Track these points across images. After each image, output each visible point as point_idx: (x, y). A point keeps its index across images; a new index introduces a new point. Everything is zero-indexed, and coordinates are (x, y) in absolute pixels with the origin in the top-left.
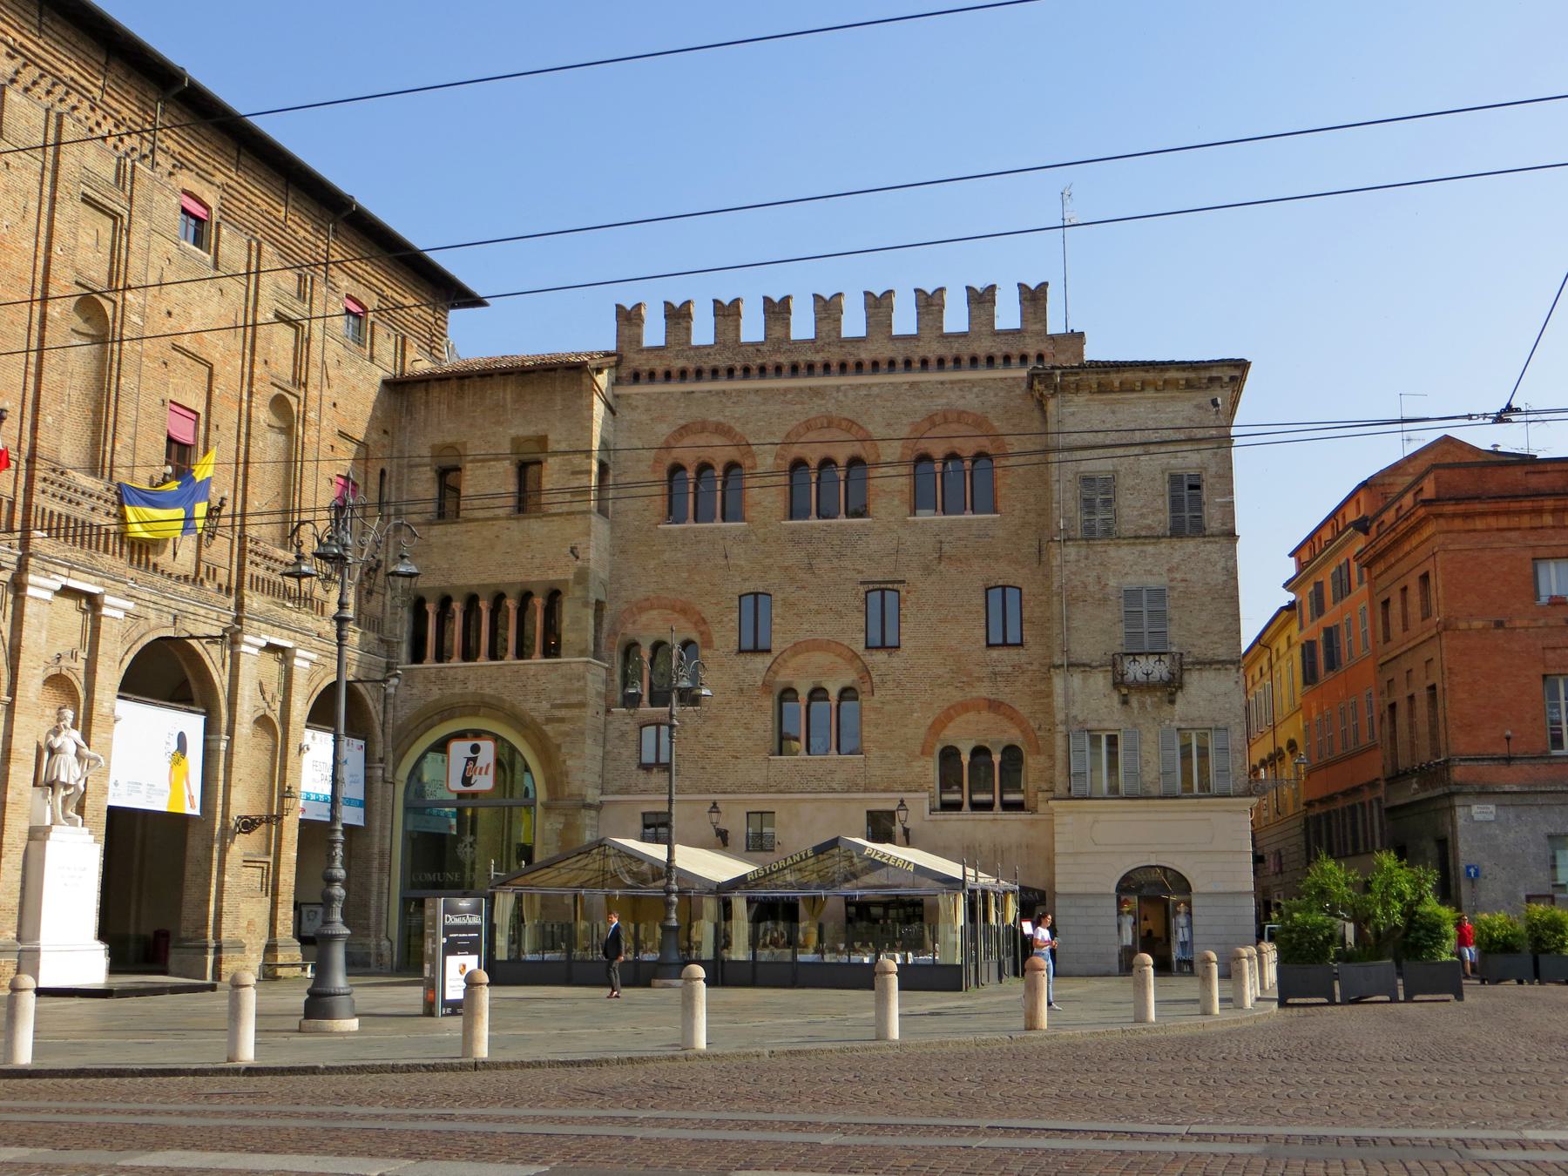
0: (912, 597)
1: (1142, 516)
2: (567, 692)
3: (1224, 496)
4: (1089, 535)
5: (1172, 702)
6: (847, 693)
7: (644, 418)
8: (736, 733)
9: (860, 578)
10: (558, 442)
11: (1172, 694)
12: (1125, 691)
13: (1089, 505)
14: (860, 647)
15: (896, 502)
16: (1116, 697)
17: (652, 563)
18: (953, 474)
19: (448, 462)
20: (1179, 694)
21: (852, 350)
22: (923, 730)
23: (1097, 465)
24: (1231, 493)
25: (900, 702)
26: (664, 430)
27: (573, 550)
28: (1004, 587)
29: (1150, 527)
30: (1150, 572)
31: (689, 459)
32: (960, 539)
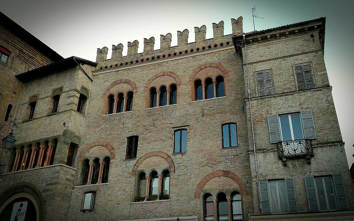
0: (192, 131)
1: (285, 84)
2: (52, 178)
3: (322, 71)
4: (262, 97)
5: (309, 163)
6: (166, 173)
7: (102, 81)
8: (120, 193)
9: (172, 126)
10: (66, 88)
11: (309, 159)
12: (284, 160)
13: (261, 82)
14: (170, 153)
15: (187, 97)
16: (280, 164)
17: (97, 130)
18: (208, 86)
19: (33, 100)
20: (312, 159)
21: (173, 50)
22: (195, 186)
23: (260, 67)
24: (325, 70)
25: (186, 174)
26: (108, 84)
27: (64, 123)
28: (229, 124)
29: (289, 88)
30: (291, 107)
31: (115, 91)
32: (211, 107)
